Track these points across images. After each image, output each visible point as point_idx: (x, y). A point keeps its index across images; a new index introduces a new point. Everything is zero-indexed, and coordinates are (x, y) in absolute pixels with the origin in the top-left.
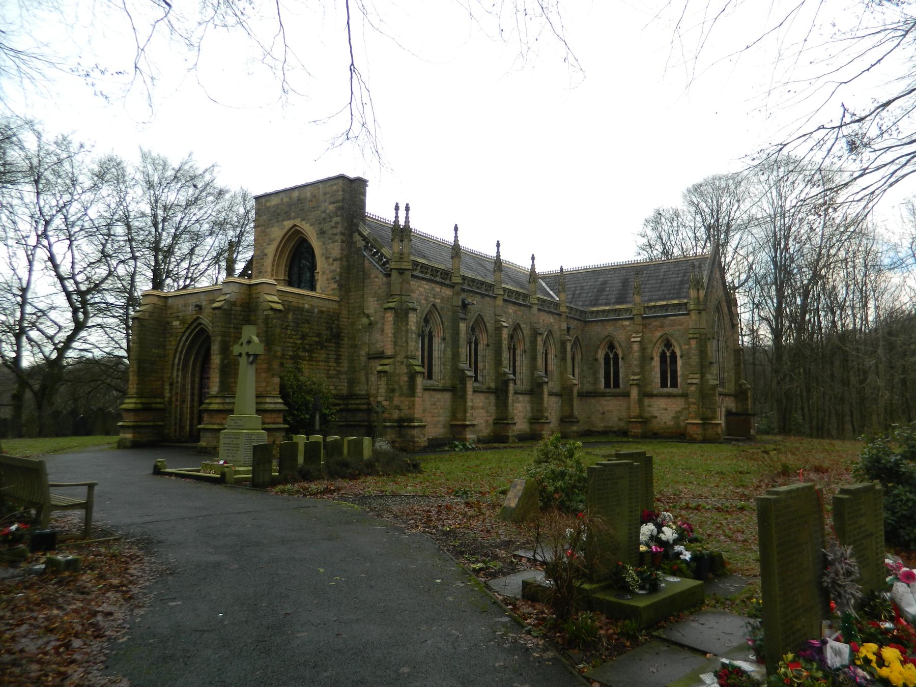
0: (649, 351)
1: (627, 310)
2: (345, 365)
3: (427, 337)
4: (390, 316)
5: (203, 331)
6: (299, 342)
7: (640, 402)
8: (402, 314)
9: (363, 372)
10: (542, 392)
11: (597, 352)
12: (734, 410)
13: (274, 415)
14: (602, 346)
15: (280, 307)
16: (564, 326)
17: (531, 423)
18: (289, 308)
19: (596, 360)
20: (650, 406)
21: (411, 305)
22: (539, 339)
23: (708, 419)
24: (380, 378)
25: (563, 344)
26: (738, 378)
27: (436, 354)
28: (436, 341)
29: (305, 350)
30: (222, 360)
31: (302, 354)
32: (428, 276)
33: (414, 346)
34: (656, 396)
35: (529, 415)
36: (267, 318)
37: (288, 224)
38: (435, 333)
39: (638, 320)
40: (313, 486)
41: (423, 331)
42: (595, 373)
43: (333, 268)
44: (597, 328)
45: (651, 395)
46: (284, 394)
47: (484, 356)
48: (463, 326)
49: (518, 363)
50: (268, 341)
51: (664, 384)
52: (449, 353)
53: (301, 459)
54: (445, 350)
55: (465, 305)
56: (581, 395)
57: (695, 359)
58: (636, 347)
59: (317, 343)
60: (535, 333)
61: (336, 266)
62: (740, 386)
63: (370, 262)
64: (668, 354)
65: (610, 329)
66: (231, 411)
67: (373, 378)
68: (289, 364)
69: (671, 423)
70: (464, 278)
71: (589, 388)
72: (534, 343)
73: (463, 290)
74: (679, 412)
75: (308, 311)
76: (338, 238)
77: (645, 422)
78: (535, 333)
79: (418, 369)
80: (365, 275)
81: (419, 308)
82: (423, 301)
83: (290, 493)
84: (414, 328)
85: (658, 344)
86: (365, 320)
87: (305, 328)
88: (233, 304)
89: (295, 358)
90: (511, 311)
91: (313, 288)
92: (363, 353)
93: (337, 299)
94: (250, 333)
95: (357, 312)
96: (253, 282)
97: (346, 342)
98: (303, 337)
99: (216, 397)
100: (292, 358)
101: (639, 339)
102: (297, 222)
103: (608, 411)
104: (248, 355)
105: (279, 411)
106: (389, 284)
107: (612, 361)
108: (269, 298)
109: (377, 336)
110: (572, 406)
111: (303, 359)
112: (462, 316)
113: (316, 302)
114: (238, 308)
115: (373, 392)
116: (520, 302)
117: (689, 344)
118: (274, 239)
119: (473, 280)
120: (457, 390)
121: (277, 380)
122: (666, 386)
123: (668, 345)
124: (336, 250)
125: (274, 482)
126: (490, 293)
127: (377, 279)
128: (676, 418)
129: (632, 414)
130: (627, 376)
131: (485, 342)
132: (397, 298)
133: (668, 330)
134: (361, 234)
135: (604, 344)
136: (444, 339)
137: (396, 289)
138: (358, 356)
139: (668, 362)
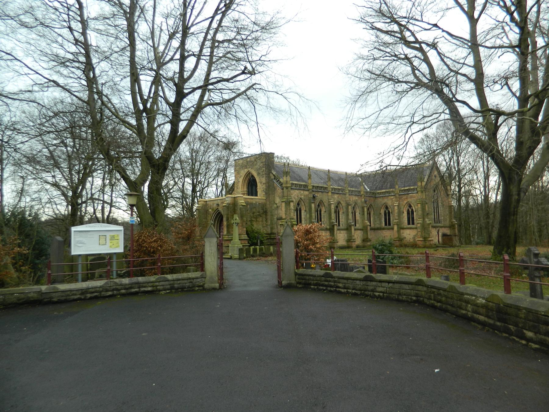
0: (402, 209)
1: (393, 191)
2: (269, 222)
3: (298, 211)
4: (284, 204)
5: (219, 213)
6: (252, 215)
7: (398, 232)
8: (288, 203)
9: (275, 225)
10: (351, 229)
11: (381, 210)
12: (449, 234)
13: (245, 241)
14: (383, 208)
15: (244, 204)
16: (363, 200)
17: (347, 242)
18: (247, 203)
19: (380, 214)
20: (403, 233)
21: (291, 200)
22: (350, 207)
23: (426, 238)
24: (281, 227)
25: (363, 208)
26: (451, 219)
27: (303, 217)
28: (303, 212)
29: (254, 218)
30: (227, 223)
31: (253, 219)
32: (298, 188)
33: (293, 215)
34: (405, 229)
35: (346, 238)
36: (240, 209)
37: (246, 170)
38: (302, 209)
39: (397, 196)
40: (254, 259)
41: (297, 208)
42: (380, 220)
43: (263, 187)
44: (380, 200)
45: (403, 229)
46: (247, 234)
47: (324, 216)
48: (313, 205)
49: (340, 218)
50: (241, 217)
51: (409, 224)
52: (308, 216)
53: (252, 253)
54: (306, 215)
55: (314, 197)
56: (371, 229)
57: (420, 212)
58: (396, 208)
59: (258, 215)
60: (348, 205)
61: (264, 186)
62: (452, 222)
63: (276, 184)
64: (387, 212)
65: (385, 200)
66: (232, 240)
67: (279, 227)
68: (249, 223)
69: (412, 240)
70: (313, 186)
71: (377, 226)
72: (347, 209)
73: (313, 191)
74: (414, 235)
75: (254, 204)
76: (265, 176)
77: (401, 240)
78: (348, 205)
79: (294, 223)
80: (275, 189)
81: (294, 200)
82: (296, 198)
83: (248, 260)
84: (292, 208)
85: (406, 206)
86: (275, 206)
87: (254, 210)
88: (229, 204)
89: (251, 221)
90: (336, 197)
91: (256, 195)
92: (275, 217)
93: (265, 198)
94: (236, 217)
95: (273, 202)
96: (236, 196)
97: (269, 214)
98: (253, 213)
99: (226, 235)
100: (250, 221)
101: (397, 204)
102: (250, 169)
103: (386, 236)
104: (236, 223)
105: (246, 239)
106: (283, 192)
107: (388, 214)
108: (241, 201)
109: (280, 211)
110: (367, 234)
111: (254, 221)
112: (312, 201)
113: (257, 200)
114: (231, 206)
115: (279, 232)
116: (340, 192)
117: (417, 206)
118: (242, 176)
119: (318, 187)
120: (331, 230)
121: (245, 229)
122: (410, 224)
123: (410, 206)
124: (264, 180)
125: (244, 258)
126: (326, 191)
127: (279, 190)
128: (414, 238)
129: (395, 237)
130: (393, 220)
131: (324, 210)
132: (286, 198)
133: (409, 200)
134: (272, 174)
135: (383, 206)
136: (306, 211)
137: (285, 194)
138: (274, 219)
139: (411, 214)
